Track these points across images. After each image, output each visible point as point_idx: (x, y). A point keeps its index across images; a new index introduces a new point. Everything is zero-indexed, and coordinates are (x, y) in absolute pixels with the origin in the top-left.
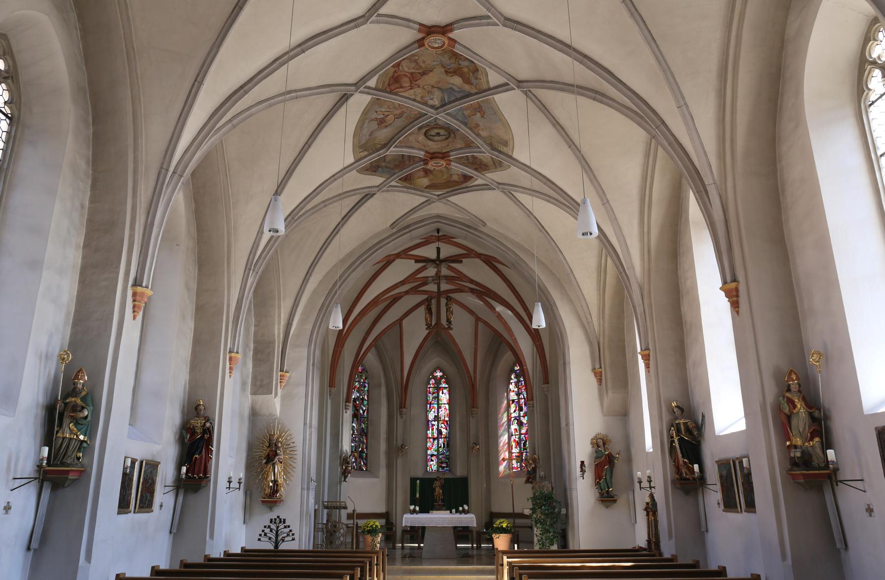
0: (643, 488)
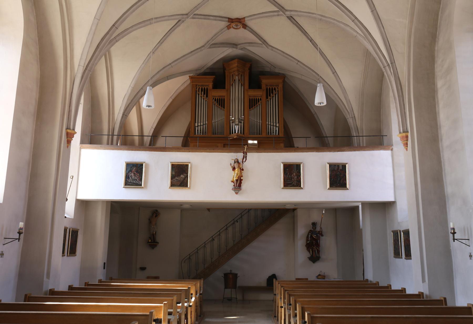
0: (456, 239)
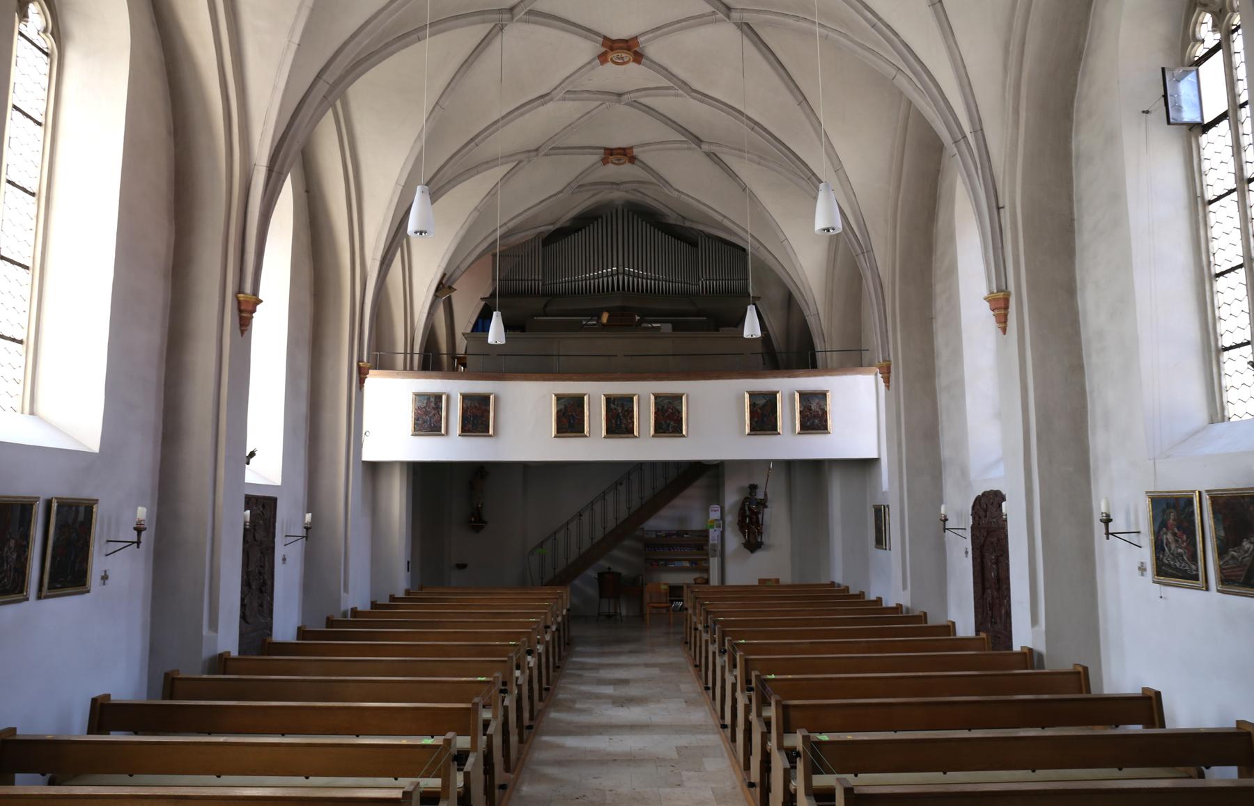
0: (1112, 534)
